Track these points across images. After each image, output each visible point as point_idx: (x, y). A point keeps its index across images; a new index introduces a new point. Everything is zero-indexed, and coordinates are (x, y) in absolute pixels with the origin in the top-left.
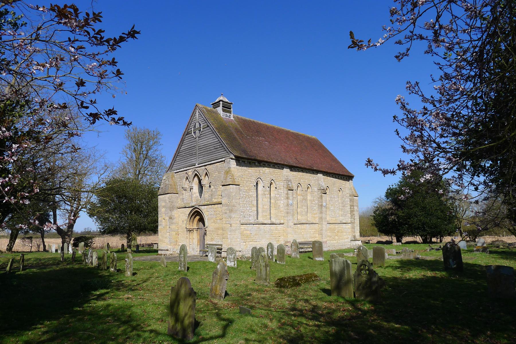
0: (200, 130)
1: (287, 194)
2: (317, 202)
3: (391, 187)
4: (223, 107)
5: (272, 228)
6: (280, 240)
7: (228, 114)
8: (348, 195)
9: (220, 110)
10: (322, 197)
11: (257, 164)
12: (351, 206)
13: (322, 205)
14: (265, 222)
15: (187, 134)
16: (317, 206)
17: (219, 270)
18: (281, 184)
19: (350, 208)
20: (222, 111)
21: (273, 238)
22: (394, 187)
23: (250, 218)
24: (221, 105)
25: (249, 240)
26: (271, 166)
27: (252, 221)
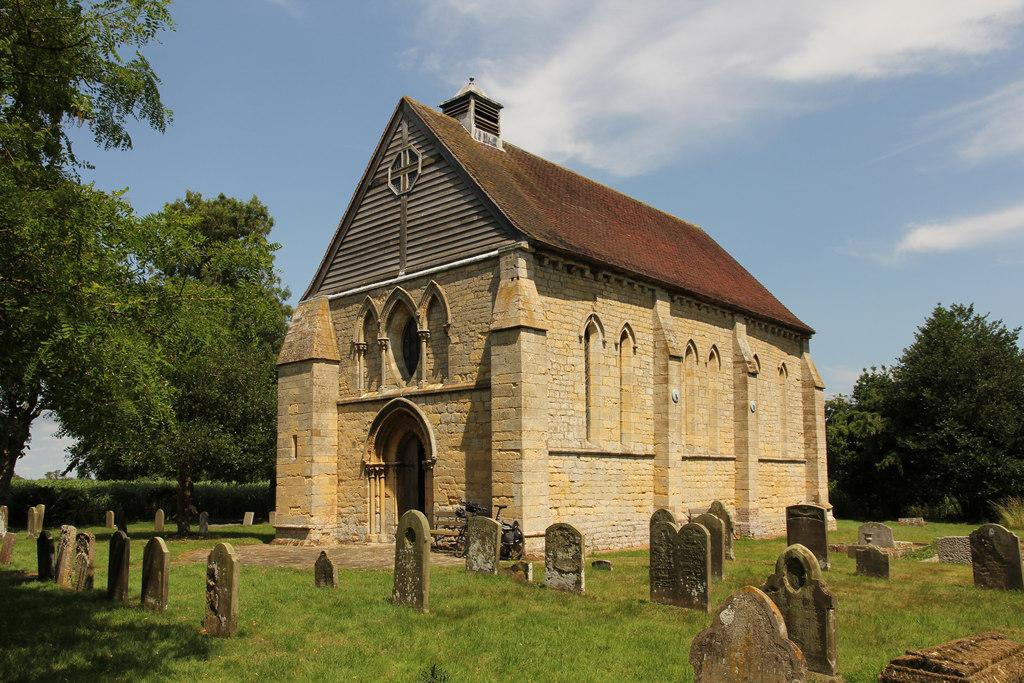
0: (412, 175)
1: (666, 368)
2: (731, 396)
3: (870, 372)
4: (477, 112)
5: (625, 467)
6: (645, 502)
7: (491, 136)
8: (799, 384)
9: (469, 120)
10: (745, 382)
11: (588, 273)
12: (806, 413)
13: (745, 407)
14: (609, 449)
15: (370, 188)
16: (732, 408)
17: (738, 633)
18: (645, 337)
19: (805, 420)
20: (473, 125)
21: (627, 497)
22: (879, 372)
23: (570, 436)
24: (472, 107)
25: (567, 503)
26: (625, 283)
27: (575, 446)
